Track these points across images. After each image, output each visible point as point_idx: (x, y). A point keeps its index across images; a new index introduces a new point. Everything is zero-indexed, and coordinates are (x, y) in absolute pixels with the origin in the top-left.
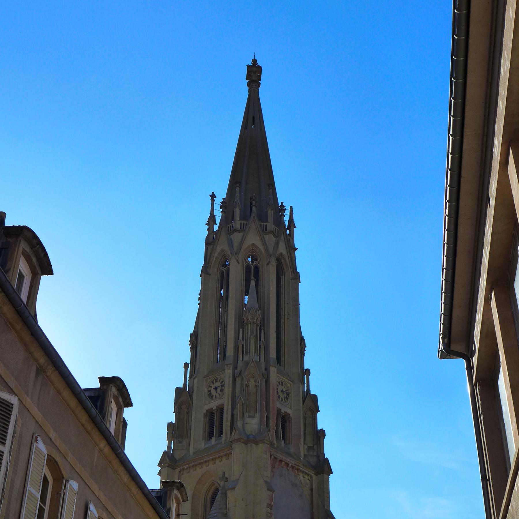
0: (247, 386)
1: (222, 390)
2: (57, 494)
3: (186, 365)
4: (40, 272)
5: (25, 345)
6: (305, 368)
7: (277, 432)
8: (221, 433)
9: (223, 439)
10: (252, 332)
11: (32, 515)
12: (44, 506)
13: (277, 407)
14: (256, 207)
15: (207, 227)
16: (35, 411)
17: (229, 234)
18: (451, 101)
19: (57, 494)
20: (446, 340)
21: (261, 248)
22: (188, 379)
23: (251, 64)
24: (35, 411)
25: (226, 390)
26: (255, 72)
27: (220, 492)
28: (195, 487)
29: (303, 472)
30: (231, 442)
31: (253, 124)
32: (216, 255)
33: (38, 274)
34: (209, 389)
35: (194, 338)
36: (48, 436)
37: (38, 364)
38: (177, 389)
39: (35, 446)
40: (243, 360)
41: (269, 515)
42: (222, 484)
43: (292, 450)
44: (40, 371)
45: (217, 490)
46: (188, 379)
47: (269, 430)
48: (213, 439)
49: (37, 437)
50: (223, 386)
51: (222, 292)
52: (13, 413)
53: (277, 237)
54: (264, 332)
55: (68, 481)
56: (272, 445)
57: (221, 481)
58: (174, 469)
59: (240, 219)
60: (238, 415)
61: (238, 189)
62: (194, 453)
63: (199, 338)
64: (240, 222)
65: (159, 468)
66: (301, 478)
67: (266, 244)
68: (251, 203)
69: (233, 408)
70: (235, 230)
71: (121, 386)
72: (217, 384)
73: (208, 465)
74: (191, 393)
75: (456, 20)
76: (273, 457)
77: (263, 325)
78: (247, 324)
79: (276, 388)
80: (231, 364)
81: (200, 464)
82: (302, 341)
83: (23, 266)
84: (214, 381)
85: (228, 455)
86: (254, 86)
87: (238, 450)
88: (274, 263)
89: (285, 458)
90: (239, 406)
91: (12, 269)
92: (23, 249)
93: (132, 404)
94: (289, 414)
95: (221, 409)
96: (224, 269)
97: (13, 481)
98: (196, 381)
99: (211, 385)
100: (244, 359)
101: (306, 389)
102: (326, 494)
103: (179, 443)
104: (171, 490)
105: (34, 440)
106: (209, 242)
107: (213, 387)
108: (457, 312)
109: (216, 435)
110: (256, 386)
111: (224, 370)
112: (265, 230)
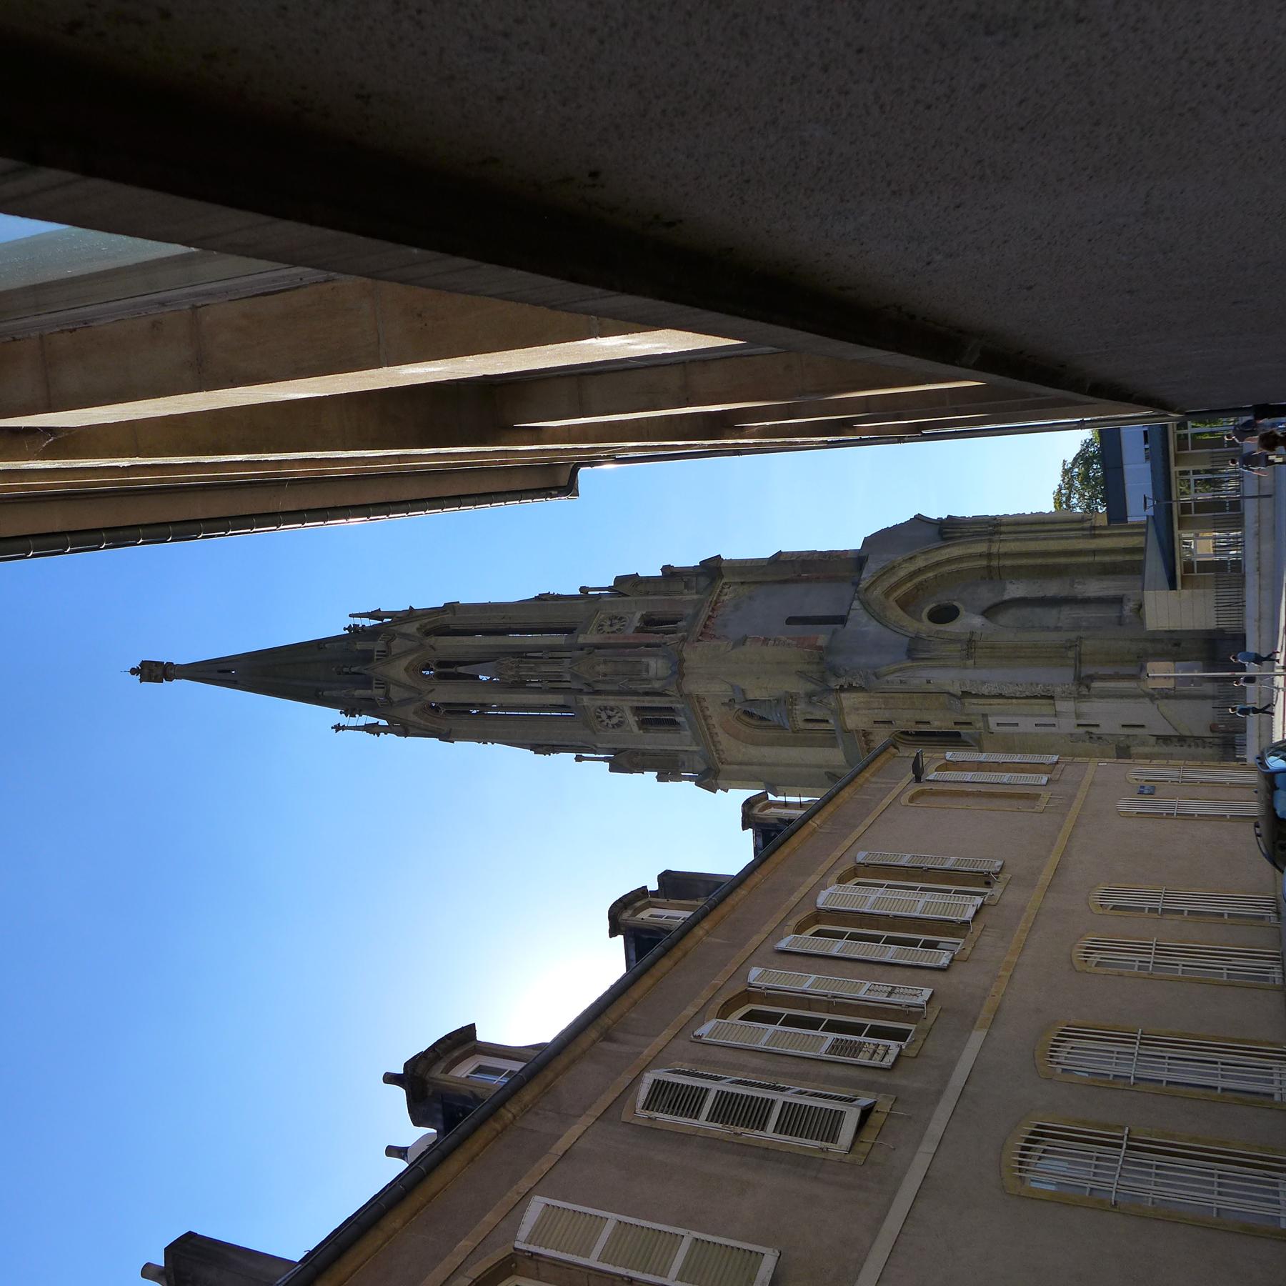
0: (605, 675)
1: (612, 710)
2: (767, 998)
3: (579, 759)
4: (473, 1044)
5: (573, 1062)
6: (579, 593)
7: (666, 633)
8: (671, 709)
9: (678, 706)
10: (531, 669)
11: (797, 1037)
12: (782, 1022)
13: (634, 632)
14: (352, 667)
15: (382, 734)
16: (660, 1041)
17: (391, 705)
18: (231, 535)
19: (767, 998)
20: (553, 492)
21: (410, 658)
22: (597, 756)
23: (139, 677)
24: (660, 1041)
25: (612, 703)
26: (151, 671)
27: (748, 709)
28: (742, 741)
29: (719, 595)
30: (681, 696)
31: (229, 671)
32: (422, 722)
33: (475, 1046)
34: (611, 726)
35: (540, 749)
36: (693, 1017)
37: (598, 1038)
38: (611, 770)
39: (706, 1039)
40: (569, 682)
41: (777, 642)
42: (737, 707)
43: (690, 611)
44: (607, 1036)
45: (746, 713)
46: (597, 756)
47: (665, 644)
48: (678, 719)
49: (695, 1037)
50: (606, 708)
51: (475, 712)
52: (666, 1080)
53: (394, 635)
54: (529, 652)
55: (749, 983)
56: (684, 639)
57: (735, 708)
58: (719, 771)
59: (369, 689)
60: (646, 687)
61: (326, 693)
62: (698, 745)
63: (540, 742)
64: (374, 688)
65: (719, 791)
66: (727, 597)
67: (405, 652)
68: (347, 673)
69: (636, 693)
70: (387, 696)
71: (620, 904)
72: (604, 716)
73: (714, 725)
74: (617, 752)
75: (118, 543)
76: (700, 638)
77: (520, 654)
78: (520, 676)
79: (608, 635)
80: (576, 698)
81: (712, 737)
82: (541, 598)
83: (463, 1071)
84: (600, 720)
85: (700, 699)
86: (172, 672)
87: (692, 686)
88: (432, 640)
89: (702, 620)
90: (633, 686)
91: (471, 1089)
92: (442, 1072)
93: (643, 887)
94: (642, 615)
95: (637, 710)
96: (443, 710)
97: (754, 1070)
98: (599, 745)
99: (605, 723)
100: (568, 680)
101: (607, 592)
102: (748, 564)
103: (684, 765)
104: (754, 817)
105: (699, 1041)
106: (405, 731)
107: (607, 721)
108: (517, 484)
109: (673, 716)
110: (605, 662)
111: (584, 706)
112: (385, 654)
